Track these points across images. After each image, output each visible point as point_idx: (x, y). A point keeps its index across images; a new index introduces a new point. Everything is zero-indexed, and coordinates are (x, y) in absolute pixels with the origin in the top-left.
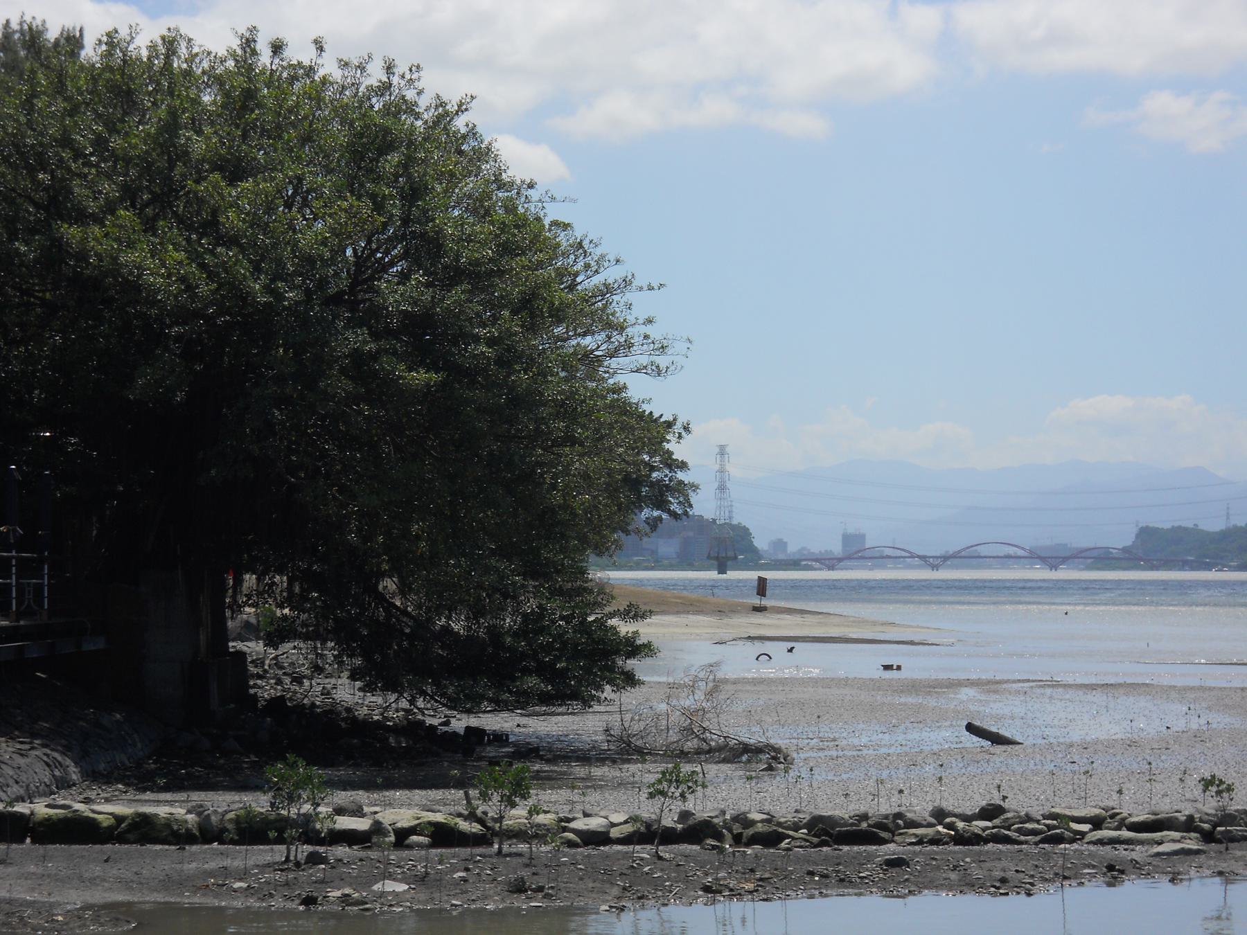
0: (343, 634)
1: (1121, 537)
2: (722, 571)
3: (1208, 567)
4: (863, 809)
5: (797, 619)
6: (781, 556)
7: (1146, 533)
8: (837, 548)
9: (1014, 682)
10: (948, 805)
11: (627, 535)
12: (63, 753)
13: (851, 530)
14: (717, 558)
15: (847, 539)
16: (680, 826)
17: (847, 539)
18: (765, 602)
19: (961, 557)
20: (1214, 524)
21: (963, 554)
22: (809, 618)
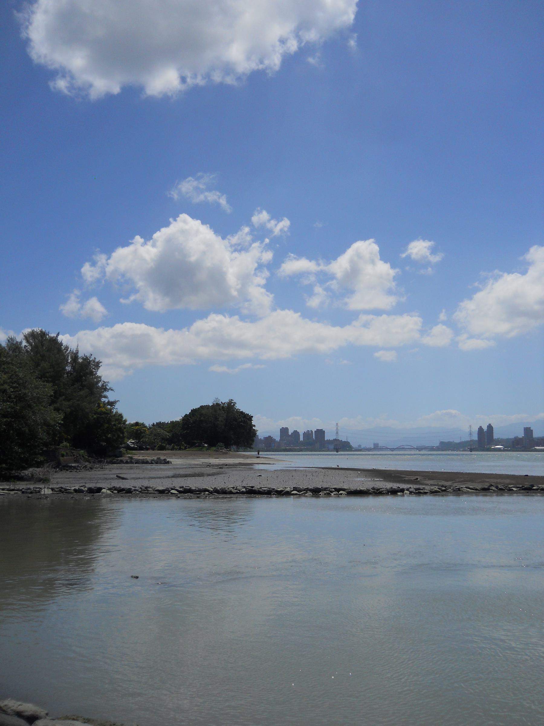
0: (17, 438)
1: (436, 444)
2: (337, 452)
3: (454, 450)
4: (114, 486)
5: (265, 459)
6: (360, 448)
7: (442, 443)
8: (372, 447)
9: (216, 468)
10: (218, 398)
11: (252, 449)
12: (144, 459)
13: (375, 443)
14: (336, 449)
15: (375, 444)
16: (476, 284)
17: (375, 444)
18: (259, 456)
19: (399, 449)
20: (458, 441)
21: (400, 447)
22: (267, 459)
